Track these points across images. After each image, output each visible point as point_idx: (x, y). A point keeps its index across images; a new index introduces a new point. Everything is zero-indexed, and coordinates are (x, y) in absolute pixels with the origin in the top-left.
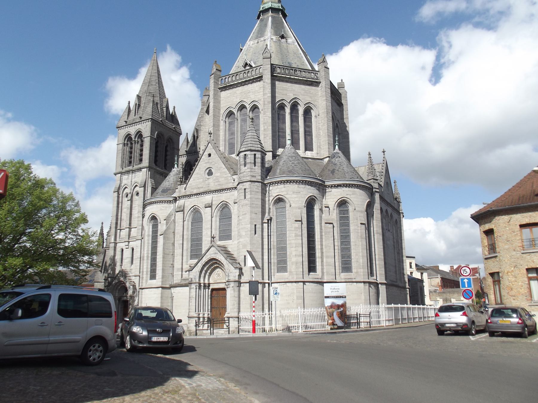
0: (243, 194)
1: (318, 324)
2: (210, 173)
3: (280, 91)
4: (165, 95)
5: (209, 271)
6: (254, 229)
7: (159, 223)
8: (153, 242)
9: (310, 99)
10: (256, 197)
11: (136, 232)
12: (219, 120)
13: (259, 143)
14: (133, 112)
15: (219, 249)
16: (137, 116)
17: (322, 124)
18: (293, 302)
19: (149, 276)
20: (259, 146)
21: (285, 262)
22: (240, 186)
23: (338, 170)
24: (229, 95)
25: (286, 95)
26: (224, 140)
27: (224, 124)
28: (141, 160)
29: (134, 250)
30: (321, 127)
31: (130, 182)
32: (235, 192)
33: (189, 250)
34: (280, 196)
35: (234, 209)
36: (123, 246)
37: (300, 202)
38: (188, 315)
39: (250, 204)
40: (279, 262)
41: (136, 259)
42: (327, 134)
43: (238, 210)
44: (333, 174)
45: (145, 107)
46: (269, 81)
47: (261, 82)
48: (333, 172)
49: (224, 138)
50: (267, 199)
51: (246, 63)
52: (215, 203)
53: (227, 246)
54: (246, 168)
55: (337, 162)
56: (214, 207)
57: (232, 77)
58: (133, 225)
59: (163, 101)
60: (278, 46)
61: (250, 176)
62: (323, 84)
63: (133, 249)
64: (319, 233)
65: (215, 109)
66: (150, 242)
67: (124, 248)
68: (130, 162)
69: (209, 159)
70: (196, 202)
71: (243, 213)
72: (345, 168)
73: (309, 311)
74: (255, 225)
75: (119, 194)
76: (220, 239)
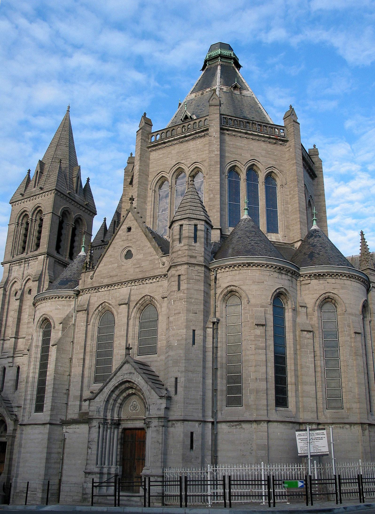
0: (177, 283)
2: (129, 255)
3: (231, 150)
4: (77, 163)
5: (119, 401)
6: (192, 337)
7: (52, 328)
8: (42, 357)
9: (274, 163)
10: (196, 287)
11: (24, 343)
12: (146, 190)
13: (202, 210)
14: (32, 182)
15: (137, 366)
16: (37, 188)
17: (291, 195)
18: (251, 453)
19: (34, 406)
20: (202, 213)
21: (239, 390)
22: (173, 271)
23: (318, 254)
24: (161, 156)
25: (241, 155)
26: (152, 216)
27: (153, 194)
28: (38, 245)
30: (289, 199)
31: (22, 275)
32: (165, 283)
33: (93, 369)
34: (232, 287)
35: (161, 307)
36: (5, 364)
37: (264, 297)
38: (86, 469)
39: (187, 298)
40: (230, 390)
42: (298, 209)
43: (168, 308)
44: (311, 259)
45: (49, 176)
46: (218, 135)
47: (207, 138)
48: (311, 256)
49: (152, 213)
50: (212, 292)
51: (186, 116)
52: (135, 298)
53: (149, 364)
54: (182, 244)
55: (317, 243)
56: (132, 305)
57: (167, 132)
58: (21, 334)
59: (73, 169)
60: (230, 97)
61: (188, 256)
62: (291, 143)
64: (292, 345)
65: (142, 174)
66: (39, 356)
67: (6, 366)
68: (24, 248)
69: (128, 235)
70: (107, 298)
71: (176, 312)
72: (328, 251)
74: (194, 331)
75: (5, 290)
76: (140, 353)
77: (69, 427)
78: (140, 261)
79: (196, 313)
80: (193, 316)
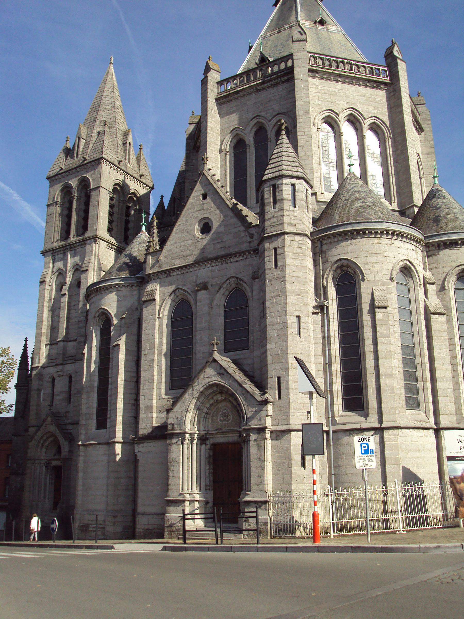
1: (416, 517)
3: (323, 97)
9: (376, 112)
25: (335, 102)
29: (73, 379)
35: (252, 291)
41: (75, 394)
63: (70, 377)
67: (55, 375)
73: (408, 489)
74: (298, 317)
77: (141, 445)
78: (221, 235)
79: (299, 295)
80: (295, 299)
